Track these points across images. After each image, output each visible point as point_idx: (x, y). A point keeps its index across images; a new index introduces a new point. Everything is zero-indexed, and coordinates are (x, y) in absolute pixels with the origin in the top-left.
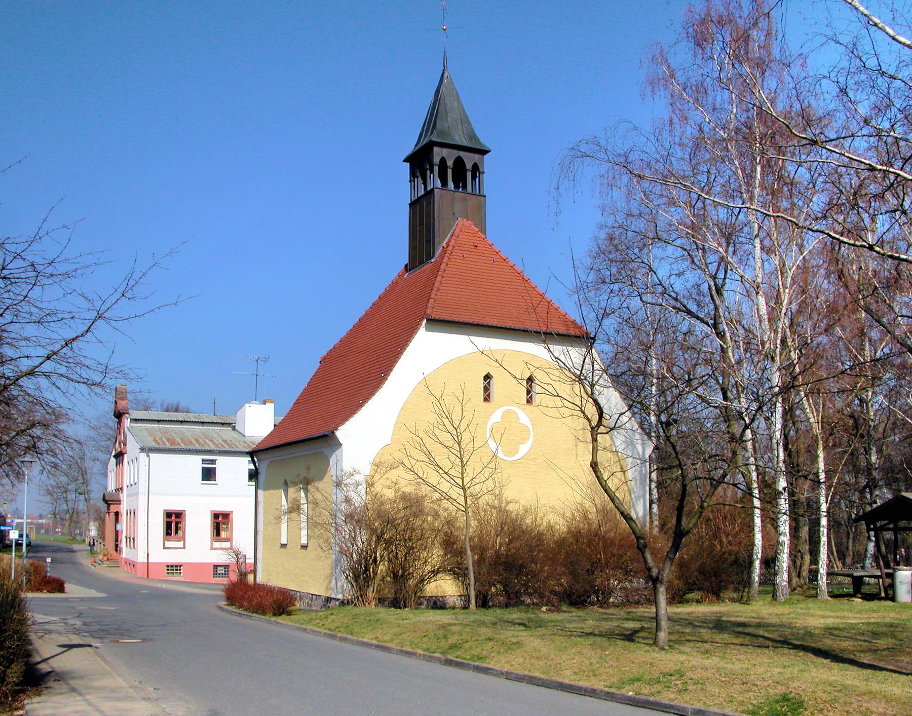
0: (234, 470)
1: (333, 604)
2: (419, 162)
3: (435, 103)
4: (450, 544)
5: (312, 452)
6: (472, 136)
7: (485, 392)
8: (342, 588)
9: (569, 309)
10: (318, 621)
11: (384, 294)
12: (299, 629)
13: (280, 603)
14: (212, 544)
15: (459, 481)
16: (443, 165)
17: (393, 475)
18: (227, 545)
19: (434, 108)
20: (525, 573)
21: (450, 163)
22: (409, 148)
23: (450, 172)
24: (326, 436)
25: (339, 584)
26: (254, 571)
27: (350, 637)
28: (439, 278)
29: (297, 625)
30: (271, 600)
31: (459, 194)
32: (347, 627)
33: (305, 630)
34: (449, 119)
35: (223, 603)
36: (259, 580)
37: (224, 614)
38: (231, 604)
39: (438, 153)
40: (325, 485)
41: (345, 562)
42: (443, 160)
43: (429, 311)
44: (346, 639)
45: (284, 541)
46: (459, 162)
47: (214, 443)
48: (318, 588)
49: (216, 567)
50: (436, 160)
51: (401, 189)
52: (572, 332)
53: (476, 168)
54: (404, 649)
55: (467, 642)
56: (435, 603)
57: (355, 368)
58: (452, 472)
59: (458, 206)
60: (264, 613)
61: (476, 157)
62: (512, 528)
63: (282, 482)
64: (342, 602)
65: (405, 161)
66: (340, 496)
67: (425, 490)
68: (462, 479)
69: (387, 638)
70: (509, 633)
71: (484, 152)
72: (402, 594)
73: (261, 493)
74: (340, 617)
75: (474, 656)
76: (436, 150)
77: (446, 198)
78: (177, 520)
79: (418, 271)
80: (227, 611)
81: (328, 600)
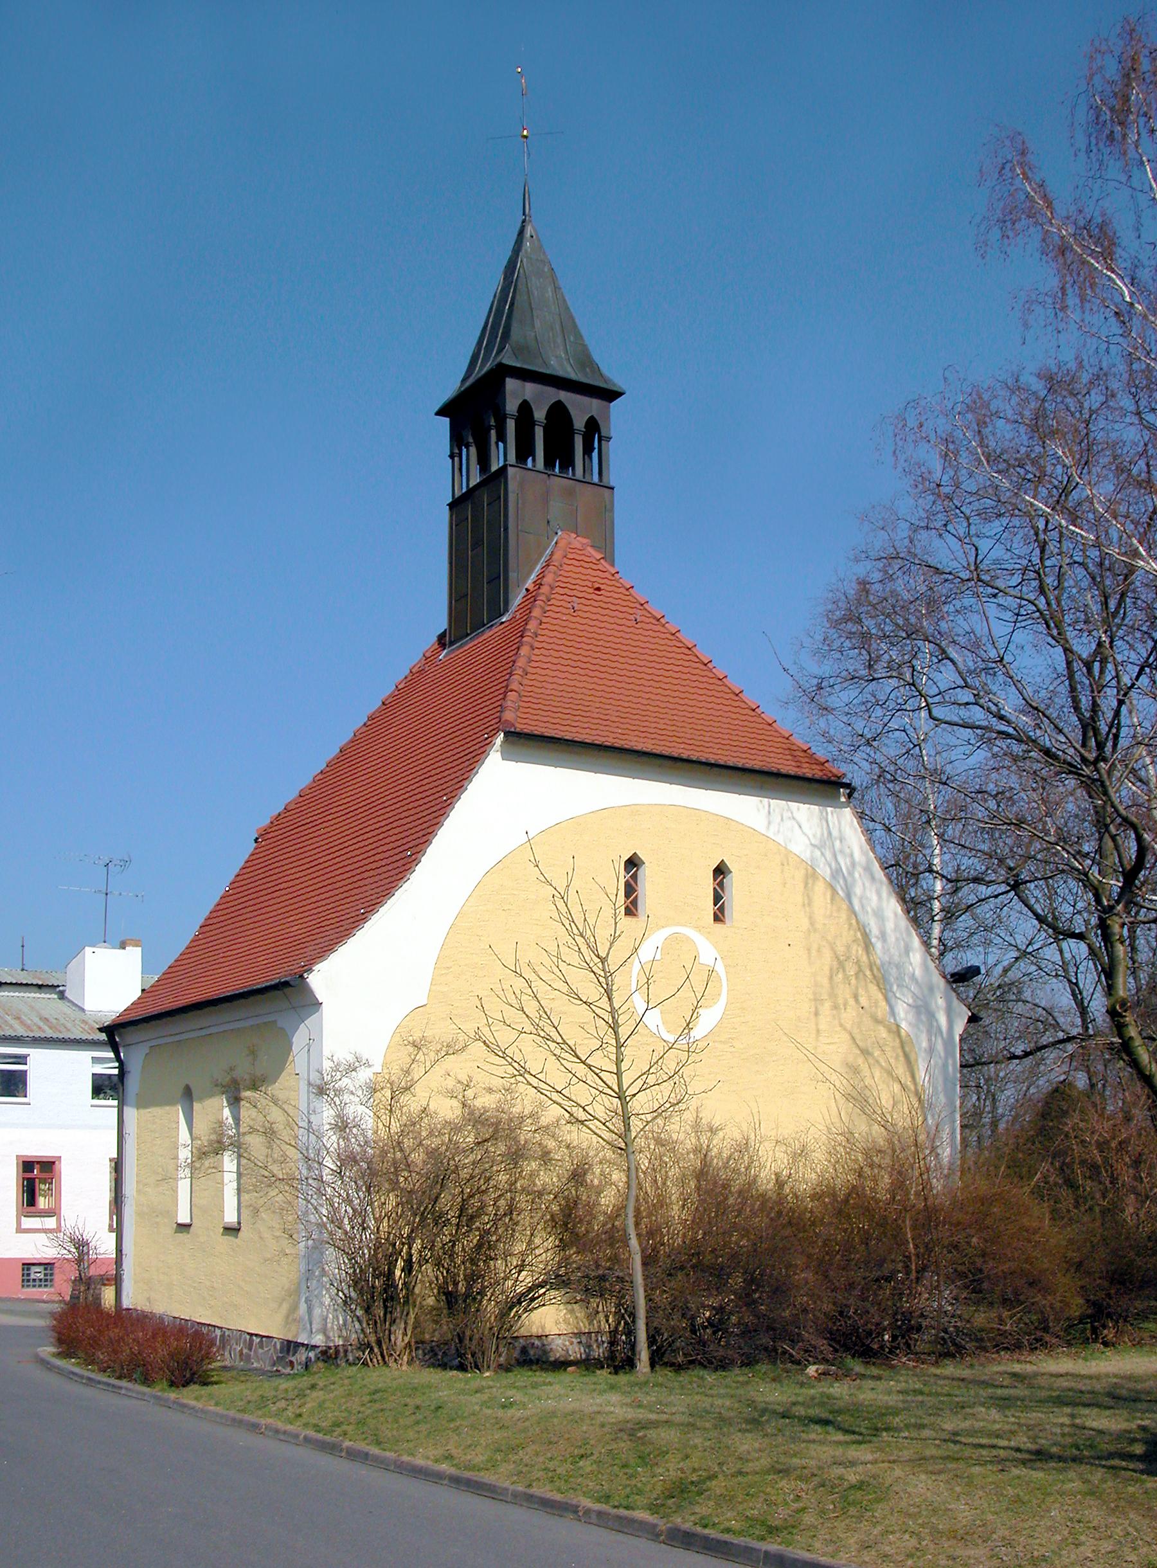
0: (62, 1078)
1: (302, 1356)
2: (472, 413)
3: (505, 291)
4: (569, 1221)
5: (251, 1022)
6: (586, 361)
7: (627, 896)
8: (328, 1321)
9: (795, 724)
10: (282, 1404)
11: (392, 695)
12: (237, 1423)
13: (181, 1357)
14: (19, 1223)
15: (612, 1080)
16: (521, 421)
17: (460, 1067)
18: (51, 1222)
19: (499, 313)
20: (761, 1292)
21: (540, 415)
22: (449, 386)
23: (539, 433)
24: (286, 984)
25: (317, 1312)
26: (117, 1281)
27: (375, 1450)
28: (524, 651)
29: (232, 1413)
30: (163, 1352)
31: (558, 483)
32: (361, 1423)
33: (254, 1427)
34: (537, 324)
35: (48, 1350)
36: (126, 1303)
37: (53, 1380)
38: (66, 1355)
39: (515, 392)
40: (291, 1085)
41: (335, 1264)
42: (525, 408)
43: (508, 715)
44: (365, 1457)
45: (184, 1218)
46: (558, 412)
47: (22, 1023)
48: (267, 1321)
49: (27, 1265)
50: (512, 406)
51: (431, 471)
52: (807, 771)
53: (593, 426)
54: (534, 1491)
55: (713, 1477)
56: (524, 1350)
57: (349, 840)
58: (596, 1060)
59: (557, 507)
60: (147, 1381)
61: (594, 406)
62: (718, 1190)
63: (179, 1091)
64: (324, 1353)
65: (440, 413)
66: (327, 1115)
67: (525, 1100)
68: (619, 1074)
69: (480, 1459)
70: (826, 1453)
71: (611, 395)
72: (465, 1337)
73: (130, 1113)
74: (332, 1395)
75: (752, 1521)
76: (511, 384)
77: (529, 487)
78: (44, 1175)
79: (469, 645)
80: (60, 1372)
81: (291, 1346)
